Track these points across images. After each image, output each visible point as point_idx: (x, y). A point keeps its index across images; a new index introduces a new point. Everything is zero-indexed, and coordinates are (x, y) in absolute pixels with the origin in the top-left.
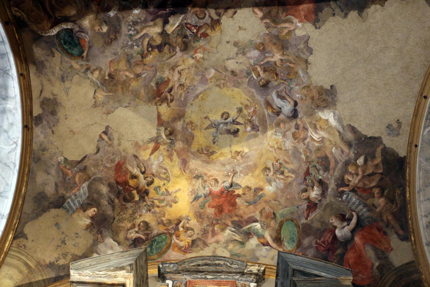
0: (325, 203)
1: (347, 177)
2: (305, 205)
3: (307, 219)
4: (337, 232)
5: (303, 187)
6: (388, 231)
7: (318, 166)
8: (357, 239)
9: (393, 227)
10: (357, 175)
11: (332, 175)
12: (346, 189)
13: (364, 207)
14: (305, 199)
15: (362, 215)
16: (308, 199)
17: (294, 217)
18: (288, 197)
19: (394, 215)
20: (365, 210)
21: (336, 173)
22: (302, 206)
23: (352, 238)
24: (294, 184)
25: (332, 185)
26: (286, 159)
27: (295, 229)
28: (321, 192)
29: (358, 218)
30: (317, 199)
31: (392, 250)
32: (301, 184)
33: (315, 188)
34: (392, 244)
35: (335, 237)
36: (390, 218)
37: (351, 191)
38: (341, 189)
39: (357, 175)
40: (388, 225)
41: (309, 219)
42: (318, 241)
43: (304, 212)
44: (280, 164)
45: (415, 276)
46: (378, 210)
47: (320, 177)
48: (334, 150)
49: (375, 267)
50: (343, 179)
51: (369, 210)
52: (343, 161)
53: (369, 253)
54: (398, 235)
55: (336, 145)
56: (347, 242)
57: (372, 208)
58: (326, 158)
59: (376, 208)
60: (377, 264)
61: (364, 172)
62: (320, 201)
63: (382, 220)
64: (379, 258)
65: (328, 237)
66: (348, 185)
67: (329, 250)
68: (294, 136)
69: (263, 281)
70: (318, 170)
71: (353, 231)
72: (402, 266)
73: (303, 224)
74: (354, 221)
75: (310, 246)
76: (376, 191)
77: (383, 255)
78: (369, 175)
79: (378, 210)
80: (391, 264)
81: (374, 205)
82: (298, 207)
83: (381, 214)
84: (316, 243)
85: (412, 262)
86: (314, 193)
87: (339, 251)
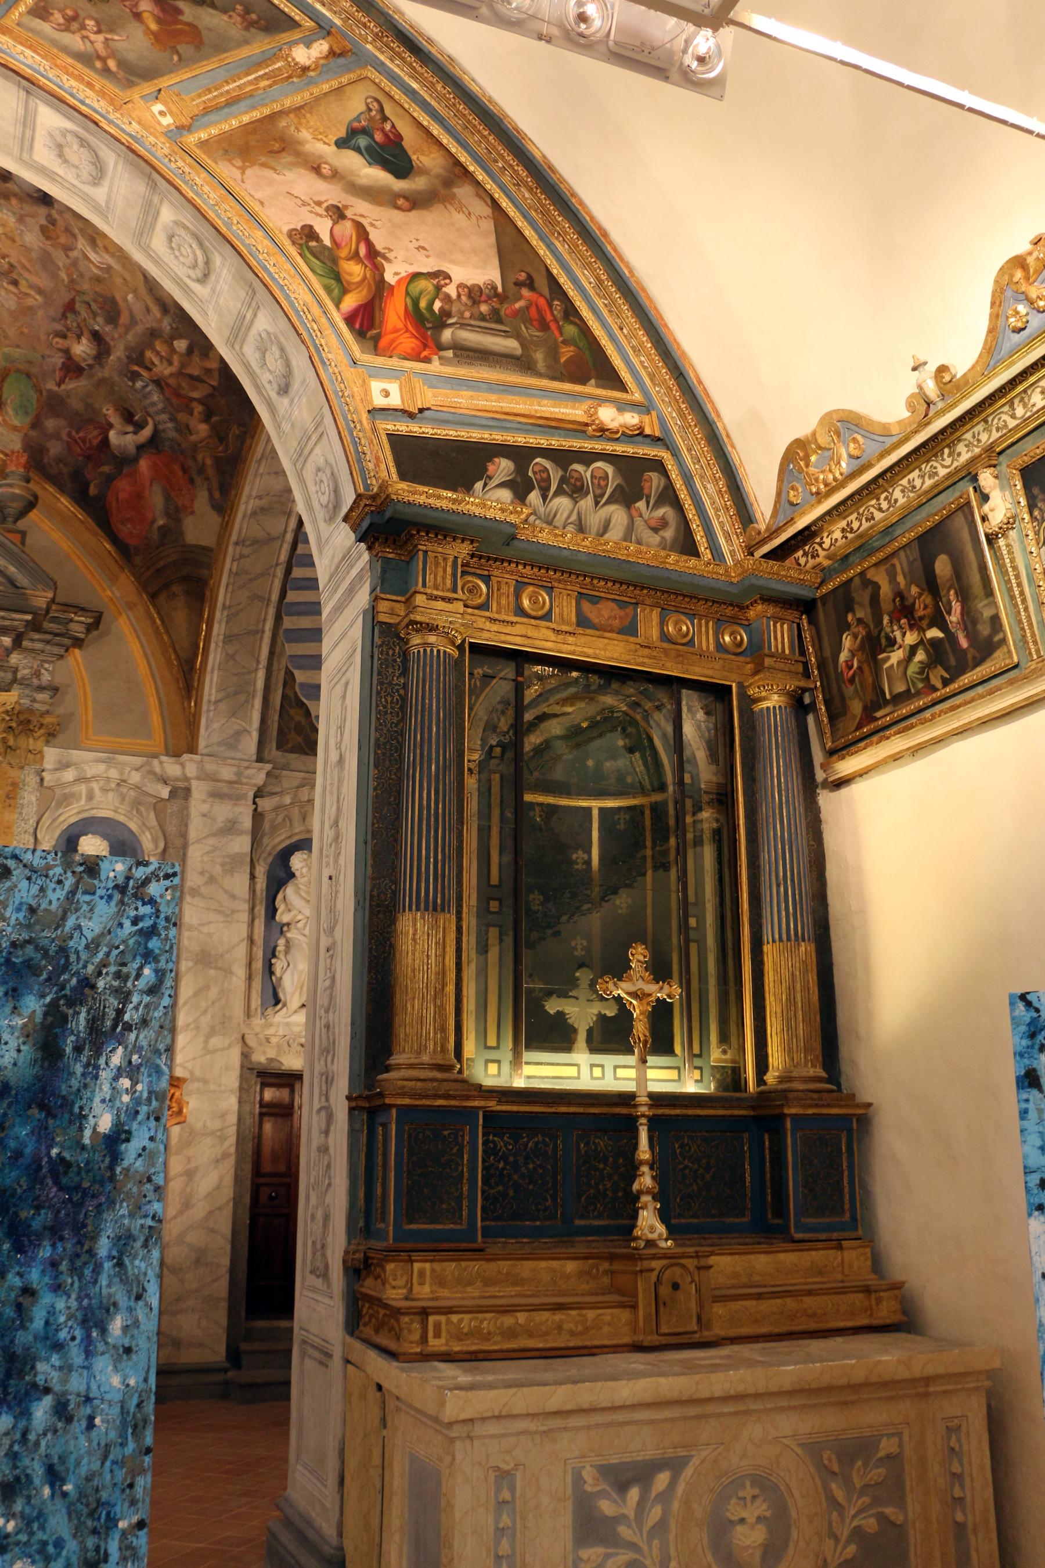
0: (100, 375)
1: (149, 354)
2: (58, 360)
3: (59, 385)
4: (112, 434)
5: (59, 327)
6: (198, 480)
7: (94, 307)
8: (144, 465)
9: (207, 479)
10: (170, 363)
11: (121, 336)
12: (144, 373)
13: (171, 420)
14: (60, 350)
15: (164, 431)
16: (67, 352)
17: (34, 370)
18: (26, 331)
19: (217, 461)
20: (170, 425)
21: (129, 337)
22: (53, 360)
23: (135, 460)
24: (40, 313)
25: (118, 353)
26: (24, 261)
27: (34, 396)
28: (94, 352)
29: (156, 431)
30: (85, 360)
31: (192, 513)
32: (54, 320)
33: (84, 340)
34: (197, 505)
35: (105, 442)
36: (209, 462)
37: (154, 381)
38: (136, 368)
39: (170, 363)
40: (201, 470)
41: (63, 387)
42: (74, 433)
43: (54, 371)
44: (11, 265)
45: (205, 572)
46: (193, 438)
47: (97, 328)
48: (130, 297)
49: (155, 526)
50: (142, 354)
51: (178, 430)
52: (148, 326)
53: (156, 499)
54: (211, 495)
55: (135, 291)
56: (124, 462)
57: (184, 430)
58: (114, 302)
59: (191, 434)
60: (161, 522)
61: (183, 365)
62: (91, 366)
63: (194, 458)
64: (167, 515)
65: (93, 435)
66: (149, 370)
67: (89, 458)
68: (43, 229)
69: (134, 41)
70: (95, 315)
71: (140, 448)
72: (196, 546)
73: (49, 391)
74: (147, 432)
75: (57, 436)
76: (198, 409)
77: (175, 513)
78: (192, 378)
79: (193, 438)
80: (181, 534)
81: (187, 427)
82: (43, 357)
83: (195, 448)
84: (69, 435)
85: (211, 550)
86: (82, 349)
87: (106, 469)
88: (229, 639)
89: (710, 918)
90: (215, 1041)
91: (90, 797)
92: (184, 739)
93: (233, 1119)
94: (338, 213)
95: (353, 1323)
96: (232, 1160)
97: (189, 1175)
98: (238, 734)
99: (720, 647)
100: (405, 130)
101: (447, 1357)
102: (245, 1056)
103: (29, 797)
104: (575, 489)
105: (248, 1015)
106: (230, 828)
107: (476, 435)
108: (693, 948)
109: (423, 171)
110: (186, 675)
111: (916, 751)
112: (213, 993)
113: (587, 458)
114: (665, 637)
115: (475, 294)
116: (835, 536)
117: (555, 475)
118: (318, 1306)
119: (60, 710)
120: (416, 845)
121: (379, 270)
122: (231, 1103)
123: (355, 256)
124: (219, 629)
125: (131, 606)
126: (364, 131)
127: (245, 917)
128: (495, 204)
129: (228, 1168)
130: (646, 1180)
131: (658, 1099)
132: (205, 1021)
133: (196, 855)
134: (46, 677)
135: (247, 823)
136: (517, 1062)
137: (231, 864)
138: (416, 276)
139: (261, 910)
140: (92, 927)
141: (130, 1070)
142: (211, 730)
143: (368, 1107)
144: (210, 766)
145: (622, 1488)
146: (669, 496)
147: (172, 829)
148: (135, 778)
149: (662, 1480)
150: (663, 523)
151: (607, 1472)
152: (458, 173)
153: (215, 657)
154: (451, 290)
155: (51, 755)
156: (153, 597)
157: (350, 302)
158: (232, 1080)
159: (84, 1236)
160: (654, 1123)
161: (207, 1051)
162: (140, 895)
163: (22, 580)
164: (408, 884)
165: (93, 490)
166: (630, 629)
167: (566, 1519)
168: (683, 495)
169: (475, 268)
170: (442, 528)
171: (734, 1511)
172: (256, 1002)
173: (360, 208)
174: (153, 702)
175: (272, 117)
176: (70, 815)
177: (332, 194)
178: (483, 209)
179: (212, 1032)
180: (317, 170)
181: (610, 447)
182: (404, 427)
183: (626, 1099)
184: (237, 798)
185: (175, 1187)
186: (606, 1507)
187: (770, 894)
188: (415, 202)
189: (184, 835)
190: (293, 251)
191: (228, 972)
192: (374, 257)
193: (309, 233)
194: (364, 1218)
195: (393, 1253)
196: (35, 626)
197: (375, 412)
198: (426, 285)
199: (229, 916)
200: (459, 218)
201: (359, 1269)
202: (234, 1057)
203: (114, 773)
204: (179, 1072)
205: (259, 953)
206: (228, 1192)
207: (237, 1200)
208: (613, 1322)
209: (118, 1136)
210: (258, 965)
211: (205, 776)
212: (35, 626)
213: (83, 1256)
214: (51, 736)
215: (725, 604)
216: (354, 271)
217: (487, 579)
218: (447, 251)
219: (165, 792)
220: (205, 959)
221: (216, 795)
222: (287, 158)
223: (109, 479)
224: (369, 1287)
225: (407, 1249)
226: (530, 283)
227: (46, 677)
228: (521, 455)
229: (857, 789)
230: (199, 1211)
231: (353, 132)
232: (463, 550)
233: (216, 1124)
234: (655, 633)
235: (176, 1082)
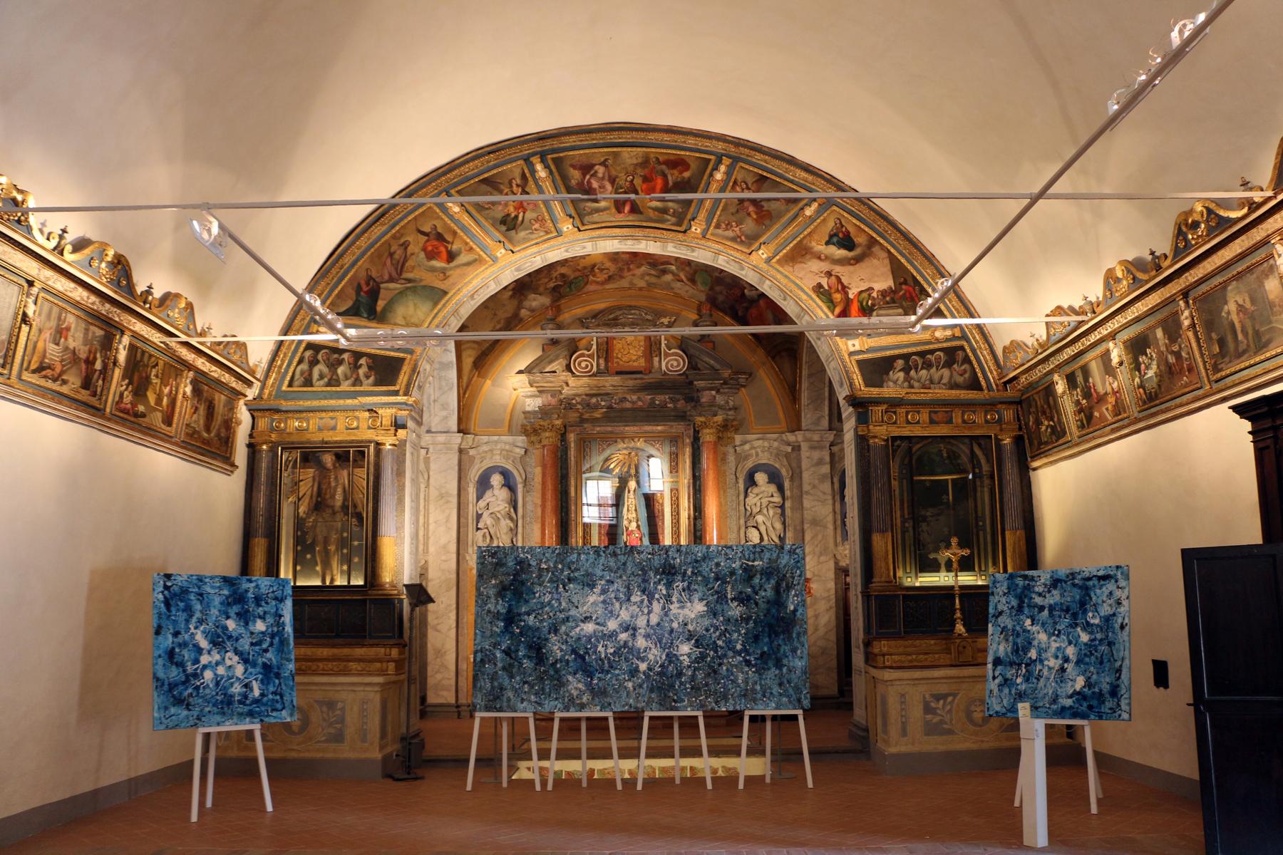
65: (738, 292)
88: (810, 376)
89: (988, 522)
90: (822, 558)
91: (757, 455)
92: (795, 426)
93: (833, 592)
94: (829, 274)
95: (867, 661)
96: (834, 610)
97: (816, 616)
98: (819, 419)
99: (987, 422)
100: (851, 229)
101: (891, 667)
102: (836, 563)
103: (731, 458)
104: (928, 365)
105: (836, 545)
106: (820, 462)
107: (888, 353)
108: (981, 533)
109: (860, 245)
110: (792, 393)
111: (1052, 463)
112: (820, 537)
113: (932, 352)
114: (964, 422)
115: (883, 293)
116: (1023, 379)
117: (920, 361)
118: (858, 658)
119: (739, 417)
120: (876, 512)
121: (846, 294)
122: (832, 585)
123: (837, 291)
124: (805, 373)
125: (764, 364)
126: (835, 235)
127: (830, 502)
128: (889, 252)
129: (832, 613)
130: (958, 615)
131: (962, 587)
132: (817, 550)
133: (805, 475)
134: (731, 403)
135: (827, 459)
136: (917, 577)
137: (822, 478)
138: (861, 292)
139: (838, 497)
140: (784, 562)
141: (796, 595)
142: (807, 419)
143: (866, 595)
144: (808, 434)
145: (938, 700)
146: (967, 360)
147: (794, 465)
148: (776, 444)
149: (950, 699)
150: (965, 371)
151: (933, 696)
152: (873, 242)
153: (805, 385)
154: (875, 295)
155: (738, 439)
156: (773, 358)
157: (837, 310)
158: (831, 575)
159: (790, 634)
160: (961, 596)
161: (819, 563)
162: (794, 553)
163: (718, 366)
164: (875, 524)
165: (740, 313)
166: (950, 421)
167: (921, 707)
168: (972, 358)
169: (883, 282)
170: (877, 402)
171: (973, 708)
172: (839, 539)
173: (838, 269)
174: (779, 407)
175: (801, 241)
176: (749, 464)
177: (825, 266)
178: (883, 255)
179: (821, 554)
180: (819, 258)
181: (940, 345)
182: (860, 357)
183: (952, 588)
184: (821, 448)
185: (811, 621)
186: (933, 705)
187: (1007, 514)
188: (857, 260)
189: (800, 467)
190: (814, 296)
191: (825, 527)
192: (844, 289)
193: (820, 286)
194: (868, 629)
195: (875, 639)
196: (725, 383)
197: (851, 354)
198: (865, 295)
199: (823, 502)
200: (875, 261)
201: (867, 644)
202: (832, 564)
203: (766, 444)
204: (809, 575)
205: (839, 517)
206: (833, 623)
207: (838, 626)
208: (945, 658)
209: (795, 610)
210: (839, 522)
211: (806, 440)
212: (725, 383)
213: (790, 638)
214: (737, 430)
215: (990, 405)
216: (838, 297)
217: (895, 413)
218: (872, 278)
219: (789, 449)
220: (815, 522)
221: (812, 448)
222: (808, 256)
223: (747, 309)
224: (870, 649)
225: (881, 637)
226: (905, 282)
227: (731, 403)
228: (906, 357)
229: (1040, 472)
230: (821, 632)
231: (831, 236)
232: (884, 407)
233: (826, 595)
234: (960, 421)
235: (807, 580)
